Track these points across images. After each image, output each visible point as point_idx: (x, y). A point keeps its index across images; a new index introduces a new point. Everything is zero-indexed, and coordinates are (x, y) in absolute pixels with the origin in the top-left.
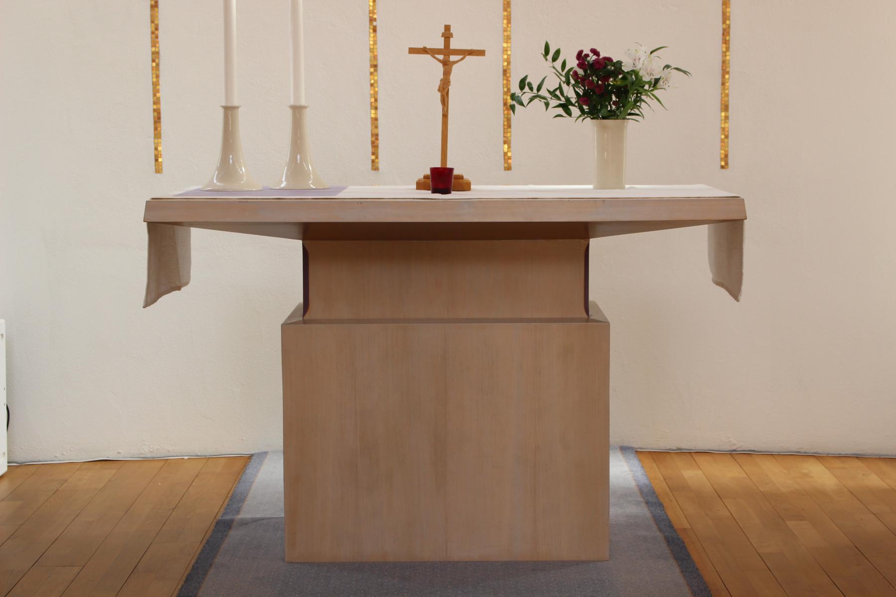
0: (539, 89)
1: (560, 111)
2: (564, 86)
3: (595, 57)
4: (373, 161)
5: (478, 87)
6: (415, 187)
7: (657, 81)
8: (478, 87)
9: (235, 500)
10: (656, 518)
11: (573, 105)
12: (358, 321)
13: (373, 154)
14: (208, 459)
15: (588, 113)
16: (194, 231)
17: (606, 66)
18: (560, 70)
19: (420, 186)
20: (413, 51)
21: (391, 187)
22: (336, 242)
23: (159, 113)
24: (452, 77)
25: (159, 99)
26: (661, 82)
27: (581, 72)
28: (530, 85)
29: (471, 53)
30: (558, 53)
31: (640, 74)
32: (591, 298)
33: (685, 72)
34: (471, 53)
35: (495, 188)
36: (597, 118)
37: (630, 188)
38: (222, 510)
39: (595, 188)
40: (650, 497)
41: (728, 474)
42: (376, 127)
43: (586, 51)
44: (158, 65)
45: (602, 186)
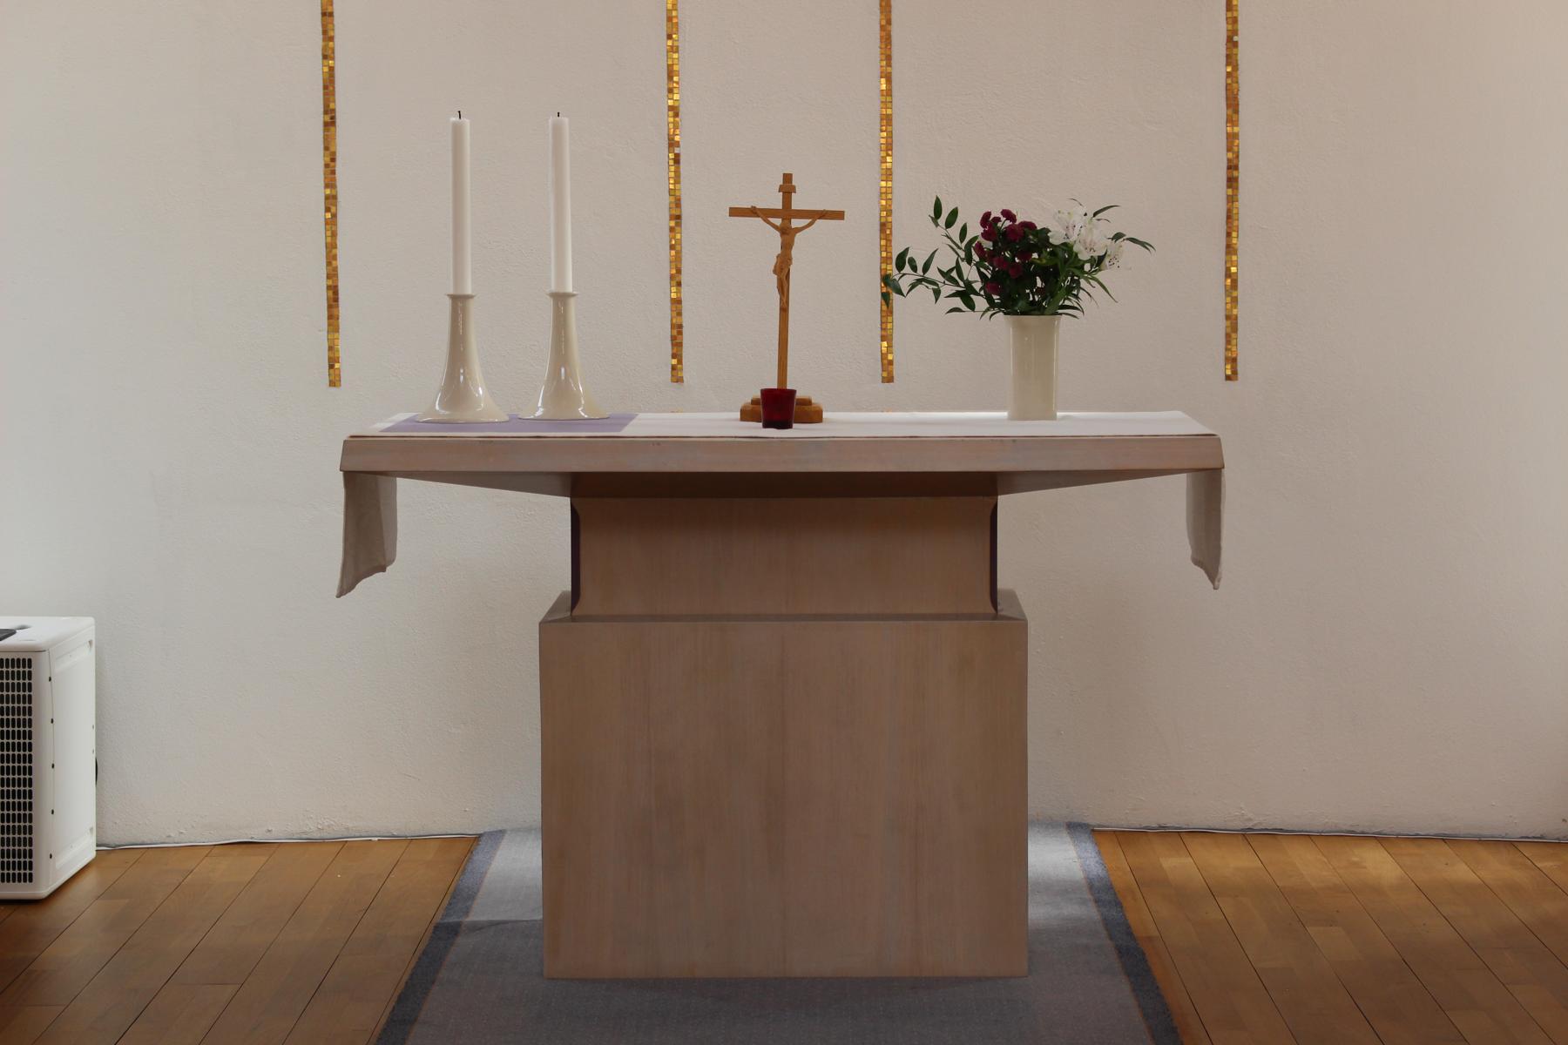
0: (926, 269)
1: (958, 302)
2: (964, 265)
3: (1008, 223)
4: (674, 368)
5: (837, 266)
6: (738, 415)
7: (1101, 259)
8: (837, 266)
9: (460, 897)
10: (1106, 922)
11: (977, 294)
12: (653, 618)
13: (674, 356)
14: (412, 840)
15: (999, 306)
16: (400, 482)
17: (1025, 236)
18: (957, 240)
19: (747, 415)
20: (735, 212)
21: (702, 418)
22: (624, 503)
23: (336, 292)
24: (794, 252)
25: (335, 269)
26: (1107, 260)
27: (988, 245)
28: (912, 261)
29: (823, 215)
30: (954, 214)
31: (1075, 249)
32: (1002, 583)
33: (1143, 244)
34: (823, 215)
35: (859, 419)
36: (1015, 313)
37: (1063, 418)
38: (441, 911)
39: (1011, 418)
40: (1103, 893)
41: (1234, 863)
42: (679, 314)
43: (996, 213)
44: (334, 216)
45: (1020, 415)
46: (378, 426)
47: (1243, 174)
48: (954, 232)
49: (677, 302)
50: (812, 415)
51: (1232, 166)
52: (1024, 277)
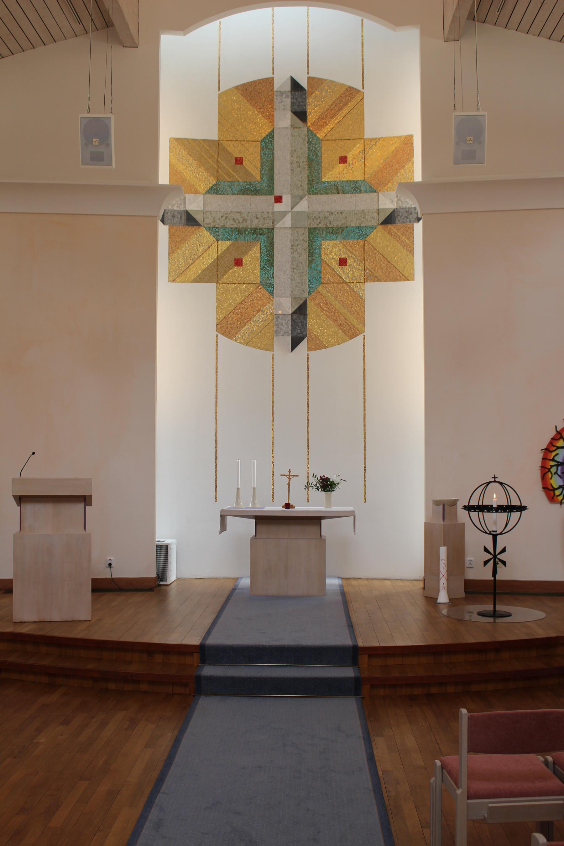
5: (298, 484)
10: (340, 590)
14: (227, 578)
22: (263, 520)
40: (341, 586)
46: (225, 508)
47: (366, 468)
48: (316, 478)
49: (273, 489)
50: (293, 507)
51: (365, 467)
52: (327, 486)
